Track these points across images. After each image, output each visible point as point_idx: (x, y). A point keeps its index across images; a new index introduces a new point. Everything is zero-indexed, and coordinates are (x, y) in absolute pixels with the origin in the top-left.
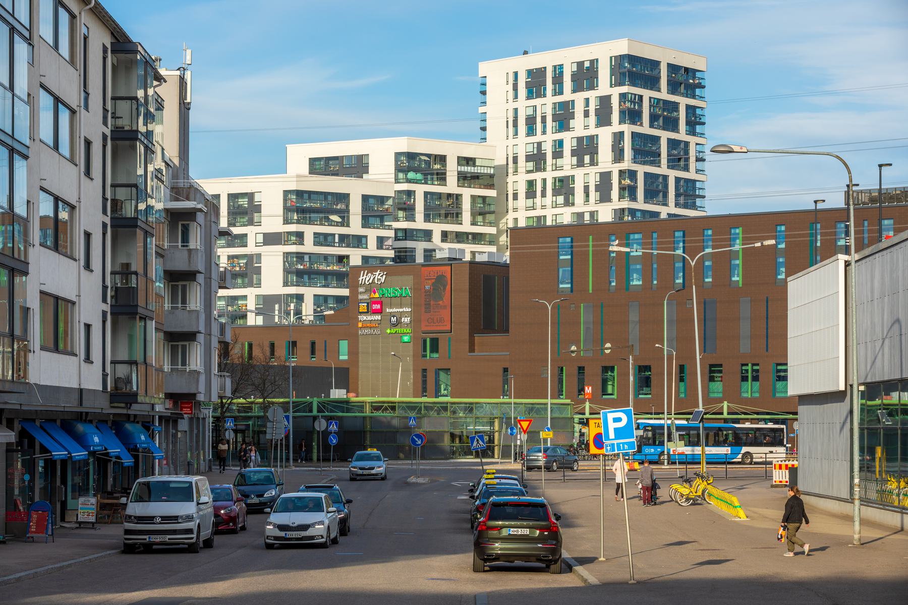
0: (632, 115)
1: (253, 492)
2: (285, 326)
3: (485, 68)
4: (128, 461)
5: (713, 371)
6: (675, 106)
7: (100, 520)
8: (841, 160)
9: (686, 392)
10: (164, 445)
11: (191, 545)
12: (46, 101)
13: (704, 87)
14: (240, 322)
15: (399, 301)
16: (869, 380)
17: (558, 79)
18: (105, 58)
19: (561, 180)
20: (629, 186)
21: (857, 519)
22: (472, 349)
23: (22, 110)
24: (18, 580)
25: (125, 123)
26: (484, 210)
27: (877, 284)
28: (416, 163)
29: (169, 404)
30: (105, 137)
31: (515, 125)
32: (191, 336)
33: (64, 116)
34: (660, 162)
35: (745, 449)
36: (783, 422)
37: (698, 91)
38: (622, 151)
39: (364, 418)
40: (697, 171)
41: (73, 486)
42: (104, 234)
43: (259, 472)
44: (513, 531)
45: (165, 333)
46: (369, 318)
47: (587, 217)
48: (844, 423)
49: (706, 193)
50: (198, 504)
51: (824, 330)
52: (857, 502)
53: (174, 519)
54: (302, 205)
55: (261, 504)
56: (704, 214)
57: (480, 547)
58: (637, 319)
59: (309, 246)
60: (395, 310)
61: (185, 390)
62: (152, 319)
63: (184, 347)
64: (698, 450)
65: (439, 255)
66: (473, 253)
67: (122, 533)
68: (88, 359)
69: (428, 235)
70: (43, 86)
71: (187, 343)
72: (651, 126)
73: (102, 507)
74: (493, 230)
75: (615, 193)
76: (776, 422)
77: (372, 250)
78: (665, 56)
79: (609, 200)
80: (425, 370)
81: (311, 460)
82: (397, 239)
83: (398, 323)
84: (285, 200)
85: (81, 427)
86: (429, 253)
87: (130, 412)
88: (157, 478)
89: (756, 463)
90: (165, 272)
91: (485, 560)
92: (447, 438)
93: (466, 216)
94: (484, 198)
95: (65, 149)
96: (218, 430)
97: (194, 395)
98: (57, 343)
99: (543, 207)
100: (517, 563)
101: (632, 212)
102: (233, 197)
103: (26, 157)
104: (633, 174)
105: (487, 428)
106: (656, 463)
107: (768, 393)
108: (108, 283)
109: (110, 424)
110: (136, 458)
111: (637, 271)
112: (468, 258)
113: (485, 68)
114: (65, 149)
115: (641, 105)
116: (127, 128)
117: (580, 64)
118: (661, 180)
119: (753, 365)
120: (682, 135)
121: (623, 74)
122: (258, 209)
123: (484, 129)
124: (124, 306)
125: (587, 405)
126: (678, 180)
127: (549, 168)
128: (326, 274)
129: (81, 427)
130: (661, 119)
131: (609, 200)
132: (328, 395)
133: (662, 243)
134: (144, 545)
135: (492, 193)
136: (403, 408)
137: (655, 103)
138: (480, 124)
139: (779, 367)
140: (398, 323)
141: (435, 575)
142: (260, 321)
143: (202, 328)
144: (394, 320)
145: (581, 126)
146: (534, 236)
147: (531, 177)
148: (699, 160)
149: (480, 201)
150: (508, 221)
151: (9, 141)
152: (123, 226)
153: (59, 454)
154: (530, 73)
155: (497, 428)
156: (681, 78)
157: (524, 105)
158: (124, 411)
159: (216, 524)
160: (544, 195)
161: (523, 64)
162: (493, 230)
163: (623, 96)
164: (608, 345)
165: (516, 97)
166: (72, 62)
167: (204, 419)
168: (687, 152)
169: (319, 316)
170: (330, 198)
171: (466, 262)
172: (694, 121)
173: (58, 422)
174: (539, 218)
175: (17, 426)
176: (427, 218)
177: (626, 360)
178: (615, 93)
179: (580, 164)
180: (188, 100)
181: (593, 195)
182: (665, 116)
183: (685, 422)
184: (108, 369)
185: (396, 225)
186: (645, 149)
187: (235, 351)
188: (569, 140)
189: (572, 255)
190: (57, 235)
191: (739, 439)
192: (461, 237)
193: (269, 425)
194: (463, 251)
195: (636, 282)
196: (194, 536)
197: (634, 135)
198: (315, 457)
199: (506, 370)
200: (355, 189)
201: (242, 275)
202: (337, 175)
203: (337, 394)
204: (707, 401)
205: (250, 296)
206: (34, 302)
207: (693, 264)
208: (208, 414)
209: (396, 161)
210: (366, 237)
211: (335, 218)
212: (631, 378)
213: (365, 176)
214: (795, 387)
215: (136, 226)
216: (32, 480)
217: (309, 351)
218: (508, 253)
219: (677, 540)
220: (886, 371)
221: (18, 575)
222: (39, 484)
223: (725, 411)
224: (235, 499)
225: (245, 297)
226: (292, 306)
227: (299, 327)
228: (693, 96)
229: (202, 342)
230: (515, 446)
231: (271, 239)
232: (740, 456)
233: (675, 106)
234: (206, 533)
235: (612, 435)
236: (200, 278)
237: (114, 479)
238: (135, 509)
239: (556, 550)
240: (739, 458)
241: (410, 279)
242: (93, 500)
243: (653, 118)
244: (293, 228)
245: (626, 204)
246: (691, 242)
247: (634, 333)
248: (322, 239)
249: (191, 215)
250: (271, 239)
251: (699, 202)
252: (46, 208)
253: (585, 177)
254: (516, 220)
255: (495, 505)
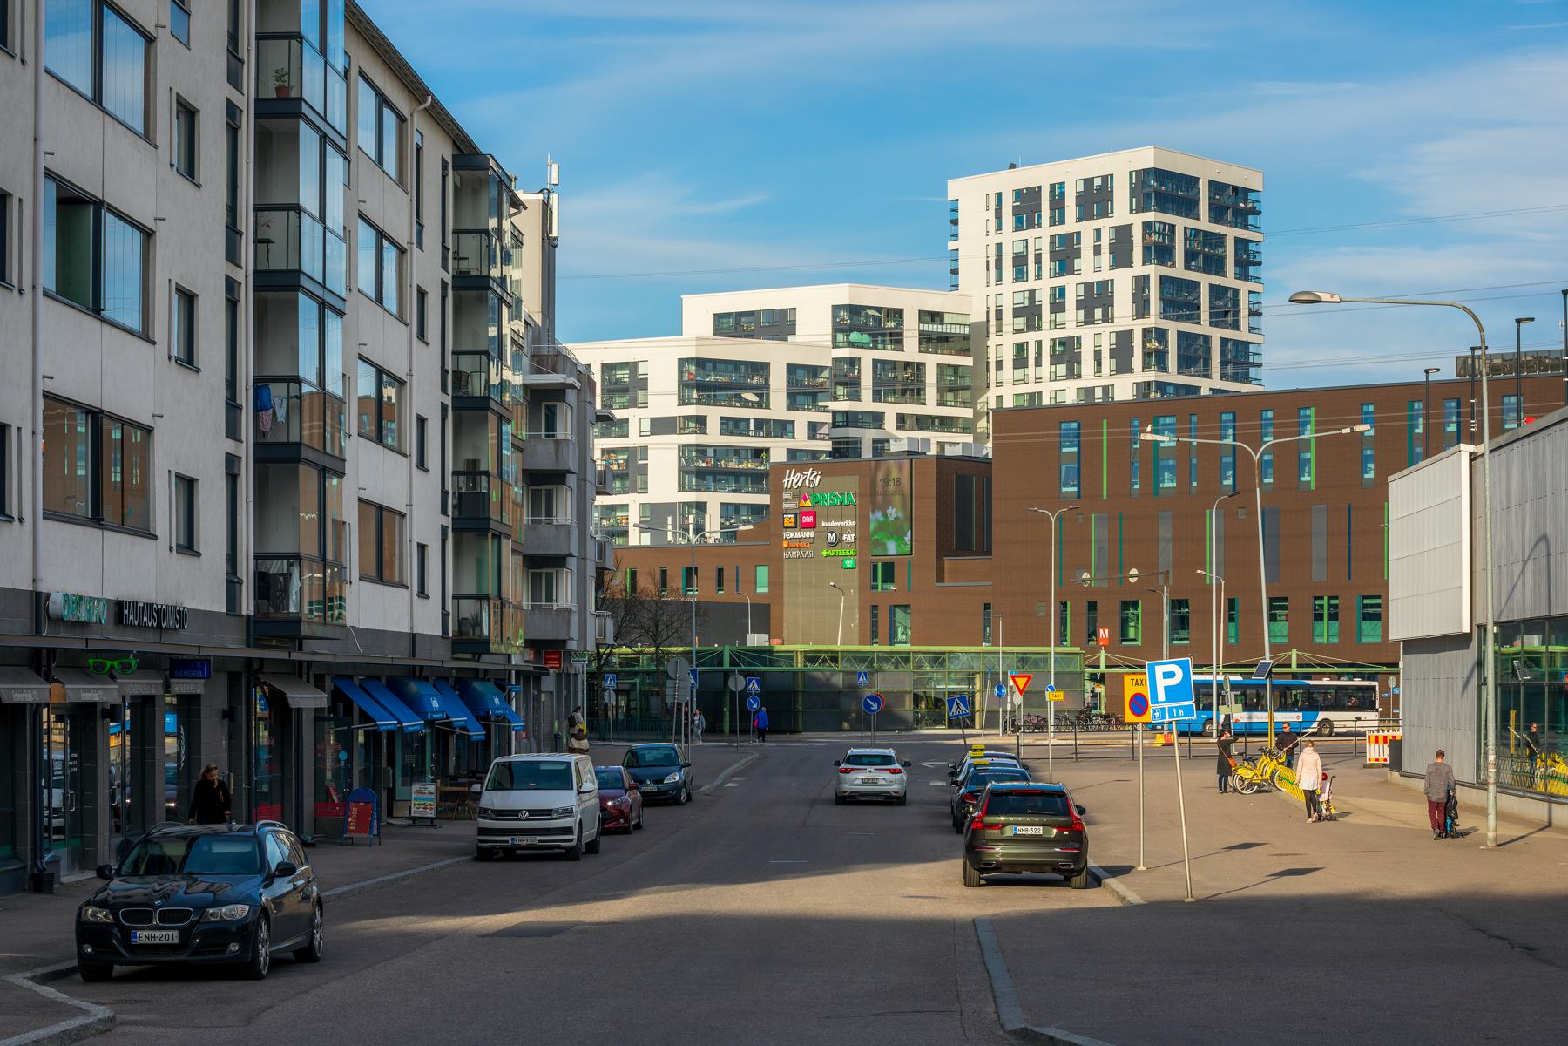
0: (1160, 252)
1: (648, 777)
2: (681, 547)
3: (956, 188)
4: (477, 734)
5: (1277, 604)
6: (1220, 240)
7: (441, 815)
8: (1470, 312)
9: (1237, 637)
10: (522, 713)
11: (569, 849)
12: (365, 235)
13: (1259, 213)
14: (619, 541)
15: (840, 511)
16: (1504, 619)
17: (1058, 203)
18: (444, 177)
19: (1063, 342)
20: (1157, 350)
21: (1492, 811)
22: (940, 578)
23: (337, 250)
24: (340, 896)
25: (472, 266)
26: (956, 385)
27: (1515, 484)
28: (862, 320)
29: (529, 655)
30: (444, 285)
31: (999, 266)
32: (559, 561)
33: (390, 255)
34: (1199, 317)
35: (1322, 715)
36: (1371, 677)
37: (1251, 219)
38: (1147, 301)
39: (795, 673)
40: (1251, 329)
41: (404, 766)
42: (443, 420)
43: (657, 748)
44: (1020, 830)
45: (525, 556)
46: (798, 535)
47: (1099, 394)
48: (1469, 678)
49: (1263, 360)
50: (579, 793)
51: (1440, 546)
52: (1492, 788)
53: (547, 813)
54: (705, 380)
55: (660, 792)
56: (1260, 389)
57: (974, 853)
58: (1169, 535)
59: (713, 436)
60: (833, 524)
61: (551, 636)
62: (508, 537)
63: (549, 576)
64: (1260, 717)
65: (894, 447)
66: (941, 445)
67: (475, 832)
68: (422, 593)
69: (878, 419)
70: (362, 216)
71: (553, 571)
72: (1187, 267)
73: (443, 796)
74: (967, 413)
75: (1137, 361)
76: (1362, 676)
77: (801, 440)
78: (1206, 171)
79: (1129, 370)
80: (875, 607)
81: (721, 731)
82: (835, 425)
83: (838, 542)
84: (681, 373)
85: (414, 687)
86: (880, 446)
87: (479, 666)
88: (515, 757)
89: (1337, 734)
90: (525, 471)
91: (982, 871)
92: (909, 701)
93: (931, 393)
94: (956, 368)
95: (391, 301)
96: (594, 692)
97: (564, 642)
98: (381, 572)
99: (1038, 380)
100: (1026, 874)
101: (1161, 386)
102: (608, 368)
103: (341, 314)
104: (1161, 334)
105: (964, 687)
106: (1200, 734)
107: (1350, 636)
108: (449, 487)
109: (452, 681)
110: (487, 728)
111: (1169, 468)
112: (934, 451)
113: (956, 188)
114: (391, 301)
115: (1172, 239)
116: (473, 273)
117: (1088, 182)
118: (1200, 341)
119: (1331, 598)
120: (1229, 280)
121: (1148, 196)
122: (643, 384)
123: (955, 272)
124: (470, 519)
125: (1103, 654)
126: (1224, 341)
127: (1045, 326)
128: (737, 475)
129: (414, 687)
130: (1201, 258)
131: (1129, 370)
132: (744, 641)
133: (1204, 429)
134: (505, 850)
135: (967, 361)
136: (848, 660)
137: (1192, 235)
138: (949, 266)
139: (1367, 601)
140: (838, 542)
141: (913, 892)
142: (646, 539)
143: (574, 550)
144: (832, 537)
145: (1090, 268)
146: (1023, 420)
147: (1021, 338)
148: (1252, 314)
149: (950, 371)
150: (990, 400)
151: (319, 291)
152: (469, 408)
153: (386, 723)
154: (1019, 194)
155: (978, 686)
156: (1227, 199)
157: (1011, 239)
158: (472, 665)
159: (602, 821)
160: (1038, 363)
161: (1009, 182)
162: (967, 413)
163: (1148, 226)
164: (1134, 571)
165: (999, 228)
166: (401, 182)
167: (576, 675)
168: (1236, 303)
169: (729, 534)
170: (742, 368)
171: (931, 457)
172: (1247, 261)
173: (384, 680)
174: (1032, 395)
175: (328, 684)
176: (877, 397)
177: (1156, 592)
178: (1137, 221)
179: (1089, 320)
180: (555, 234)
181: (1108, 364)
182: (1206, 253)
183: (1239, 678)
184: (450, 608)
185: (834, 406)
186: (1179, 299)
187: (618, 581)
188: (1073, 287)
189: (1079, 446)
190: (380, 420)
191: (1312, 701)
192: (923, 422)
193: (669, 683)
194: (927, 442)
195: (1168, 483)
196: (575, 837)
197: (1164, 280)
198: (727, 727)
199: (987, 606)
200: (777, 355)
201: (622, 476)
202: (752, 336)
203: (756, 640)
204: (1275, 648)
205: (634, 503)
206: (350, 514)
207: (1256, 458)
208: (582, 667)
209: (834, 317)
210: (792, 422)
211: (749, 396)
212: (1166, 617)
213: (790, 338)
214: (1401, 626)
215: (487, 408)
216: (350, 760)
217: (715, 583)
218: (990, 444)
219: (1242, 842)
220: (1528, 606)
221: (339, 890)
222: (358, 765)
223: (1294, 662)
224: (627, 785)
225: (625, 507)
226: (691, 519)
227: (704, 549)
228: (1245, 226)
229: (574, 568)
230: (1005, 712)
231: (661, 426)
232: (1315, 725)
233: (1220, 240)
234: (590, 833)
235: (1161, 696)
236: (572, 480)
237: (458, 758)
238: (493, 799)
239: (1080, 857)
240: (1314, 728)
241: (853, 481)
242: (432, 788)
243: (1190, 256)
244: (692, 410)
245: (1152, 375)
246: (1244, 427)
247: (1165, 556)
248: (732, 426)
249: (558, 392)
250: (661, 426)
251: (1253, 372)
252: (366, 384)
253: (1095, 338)
254: (1000, 398)
255: (995, 794)
